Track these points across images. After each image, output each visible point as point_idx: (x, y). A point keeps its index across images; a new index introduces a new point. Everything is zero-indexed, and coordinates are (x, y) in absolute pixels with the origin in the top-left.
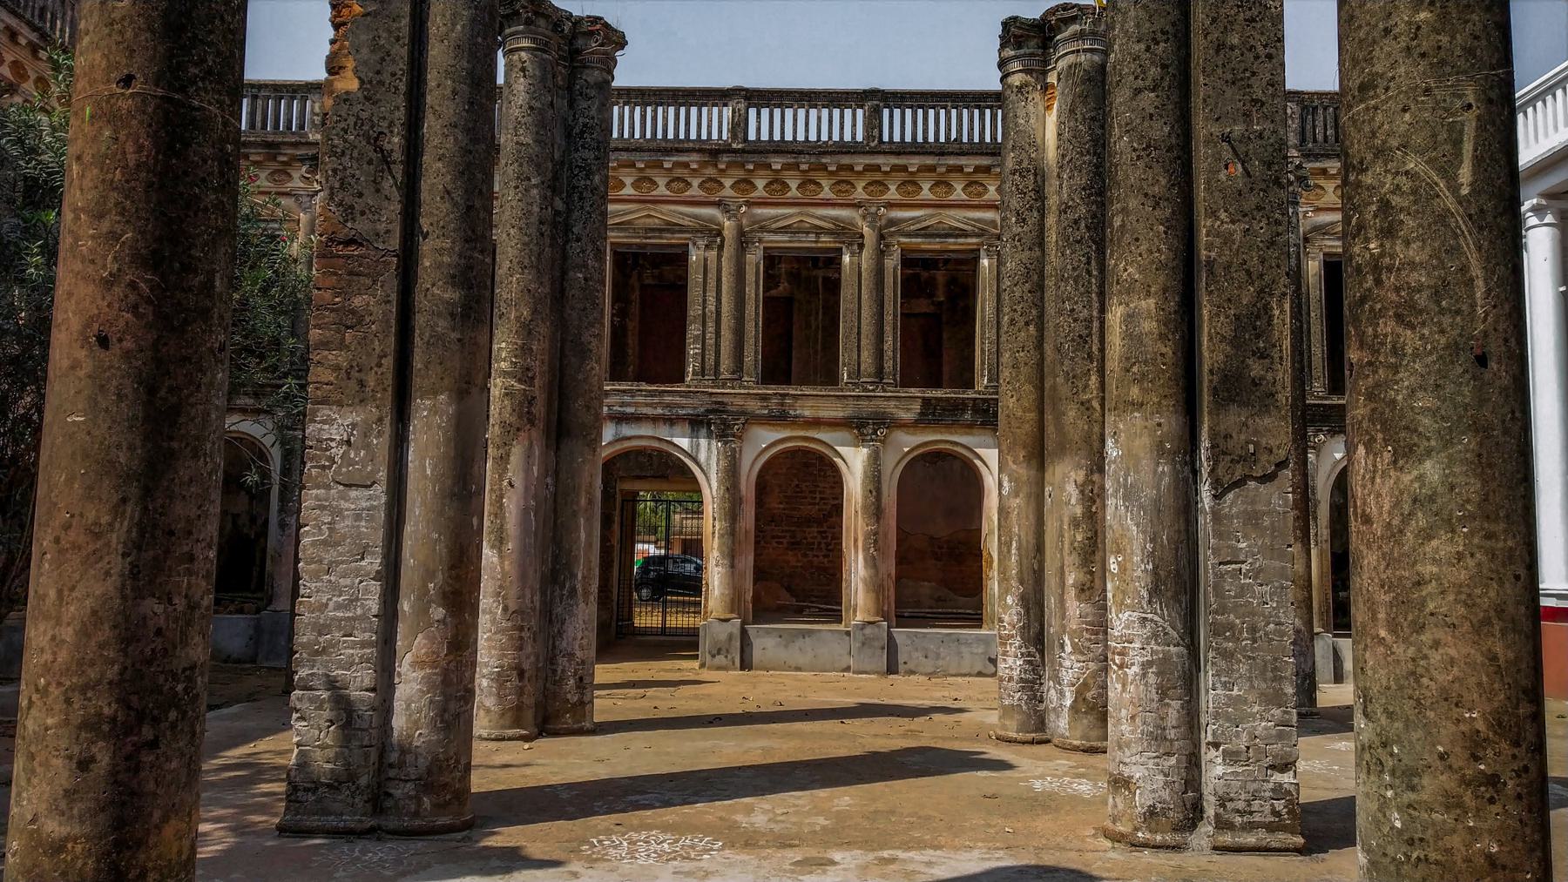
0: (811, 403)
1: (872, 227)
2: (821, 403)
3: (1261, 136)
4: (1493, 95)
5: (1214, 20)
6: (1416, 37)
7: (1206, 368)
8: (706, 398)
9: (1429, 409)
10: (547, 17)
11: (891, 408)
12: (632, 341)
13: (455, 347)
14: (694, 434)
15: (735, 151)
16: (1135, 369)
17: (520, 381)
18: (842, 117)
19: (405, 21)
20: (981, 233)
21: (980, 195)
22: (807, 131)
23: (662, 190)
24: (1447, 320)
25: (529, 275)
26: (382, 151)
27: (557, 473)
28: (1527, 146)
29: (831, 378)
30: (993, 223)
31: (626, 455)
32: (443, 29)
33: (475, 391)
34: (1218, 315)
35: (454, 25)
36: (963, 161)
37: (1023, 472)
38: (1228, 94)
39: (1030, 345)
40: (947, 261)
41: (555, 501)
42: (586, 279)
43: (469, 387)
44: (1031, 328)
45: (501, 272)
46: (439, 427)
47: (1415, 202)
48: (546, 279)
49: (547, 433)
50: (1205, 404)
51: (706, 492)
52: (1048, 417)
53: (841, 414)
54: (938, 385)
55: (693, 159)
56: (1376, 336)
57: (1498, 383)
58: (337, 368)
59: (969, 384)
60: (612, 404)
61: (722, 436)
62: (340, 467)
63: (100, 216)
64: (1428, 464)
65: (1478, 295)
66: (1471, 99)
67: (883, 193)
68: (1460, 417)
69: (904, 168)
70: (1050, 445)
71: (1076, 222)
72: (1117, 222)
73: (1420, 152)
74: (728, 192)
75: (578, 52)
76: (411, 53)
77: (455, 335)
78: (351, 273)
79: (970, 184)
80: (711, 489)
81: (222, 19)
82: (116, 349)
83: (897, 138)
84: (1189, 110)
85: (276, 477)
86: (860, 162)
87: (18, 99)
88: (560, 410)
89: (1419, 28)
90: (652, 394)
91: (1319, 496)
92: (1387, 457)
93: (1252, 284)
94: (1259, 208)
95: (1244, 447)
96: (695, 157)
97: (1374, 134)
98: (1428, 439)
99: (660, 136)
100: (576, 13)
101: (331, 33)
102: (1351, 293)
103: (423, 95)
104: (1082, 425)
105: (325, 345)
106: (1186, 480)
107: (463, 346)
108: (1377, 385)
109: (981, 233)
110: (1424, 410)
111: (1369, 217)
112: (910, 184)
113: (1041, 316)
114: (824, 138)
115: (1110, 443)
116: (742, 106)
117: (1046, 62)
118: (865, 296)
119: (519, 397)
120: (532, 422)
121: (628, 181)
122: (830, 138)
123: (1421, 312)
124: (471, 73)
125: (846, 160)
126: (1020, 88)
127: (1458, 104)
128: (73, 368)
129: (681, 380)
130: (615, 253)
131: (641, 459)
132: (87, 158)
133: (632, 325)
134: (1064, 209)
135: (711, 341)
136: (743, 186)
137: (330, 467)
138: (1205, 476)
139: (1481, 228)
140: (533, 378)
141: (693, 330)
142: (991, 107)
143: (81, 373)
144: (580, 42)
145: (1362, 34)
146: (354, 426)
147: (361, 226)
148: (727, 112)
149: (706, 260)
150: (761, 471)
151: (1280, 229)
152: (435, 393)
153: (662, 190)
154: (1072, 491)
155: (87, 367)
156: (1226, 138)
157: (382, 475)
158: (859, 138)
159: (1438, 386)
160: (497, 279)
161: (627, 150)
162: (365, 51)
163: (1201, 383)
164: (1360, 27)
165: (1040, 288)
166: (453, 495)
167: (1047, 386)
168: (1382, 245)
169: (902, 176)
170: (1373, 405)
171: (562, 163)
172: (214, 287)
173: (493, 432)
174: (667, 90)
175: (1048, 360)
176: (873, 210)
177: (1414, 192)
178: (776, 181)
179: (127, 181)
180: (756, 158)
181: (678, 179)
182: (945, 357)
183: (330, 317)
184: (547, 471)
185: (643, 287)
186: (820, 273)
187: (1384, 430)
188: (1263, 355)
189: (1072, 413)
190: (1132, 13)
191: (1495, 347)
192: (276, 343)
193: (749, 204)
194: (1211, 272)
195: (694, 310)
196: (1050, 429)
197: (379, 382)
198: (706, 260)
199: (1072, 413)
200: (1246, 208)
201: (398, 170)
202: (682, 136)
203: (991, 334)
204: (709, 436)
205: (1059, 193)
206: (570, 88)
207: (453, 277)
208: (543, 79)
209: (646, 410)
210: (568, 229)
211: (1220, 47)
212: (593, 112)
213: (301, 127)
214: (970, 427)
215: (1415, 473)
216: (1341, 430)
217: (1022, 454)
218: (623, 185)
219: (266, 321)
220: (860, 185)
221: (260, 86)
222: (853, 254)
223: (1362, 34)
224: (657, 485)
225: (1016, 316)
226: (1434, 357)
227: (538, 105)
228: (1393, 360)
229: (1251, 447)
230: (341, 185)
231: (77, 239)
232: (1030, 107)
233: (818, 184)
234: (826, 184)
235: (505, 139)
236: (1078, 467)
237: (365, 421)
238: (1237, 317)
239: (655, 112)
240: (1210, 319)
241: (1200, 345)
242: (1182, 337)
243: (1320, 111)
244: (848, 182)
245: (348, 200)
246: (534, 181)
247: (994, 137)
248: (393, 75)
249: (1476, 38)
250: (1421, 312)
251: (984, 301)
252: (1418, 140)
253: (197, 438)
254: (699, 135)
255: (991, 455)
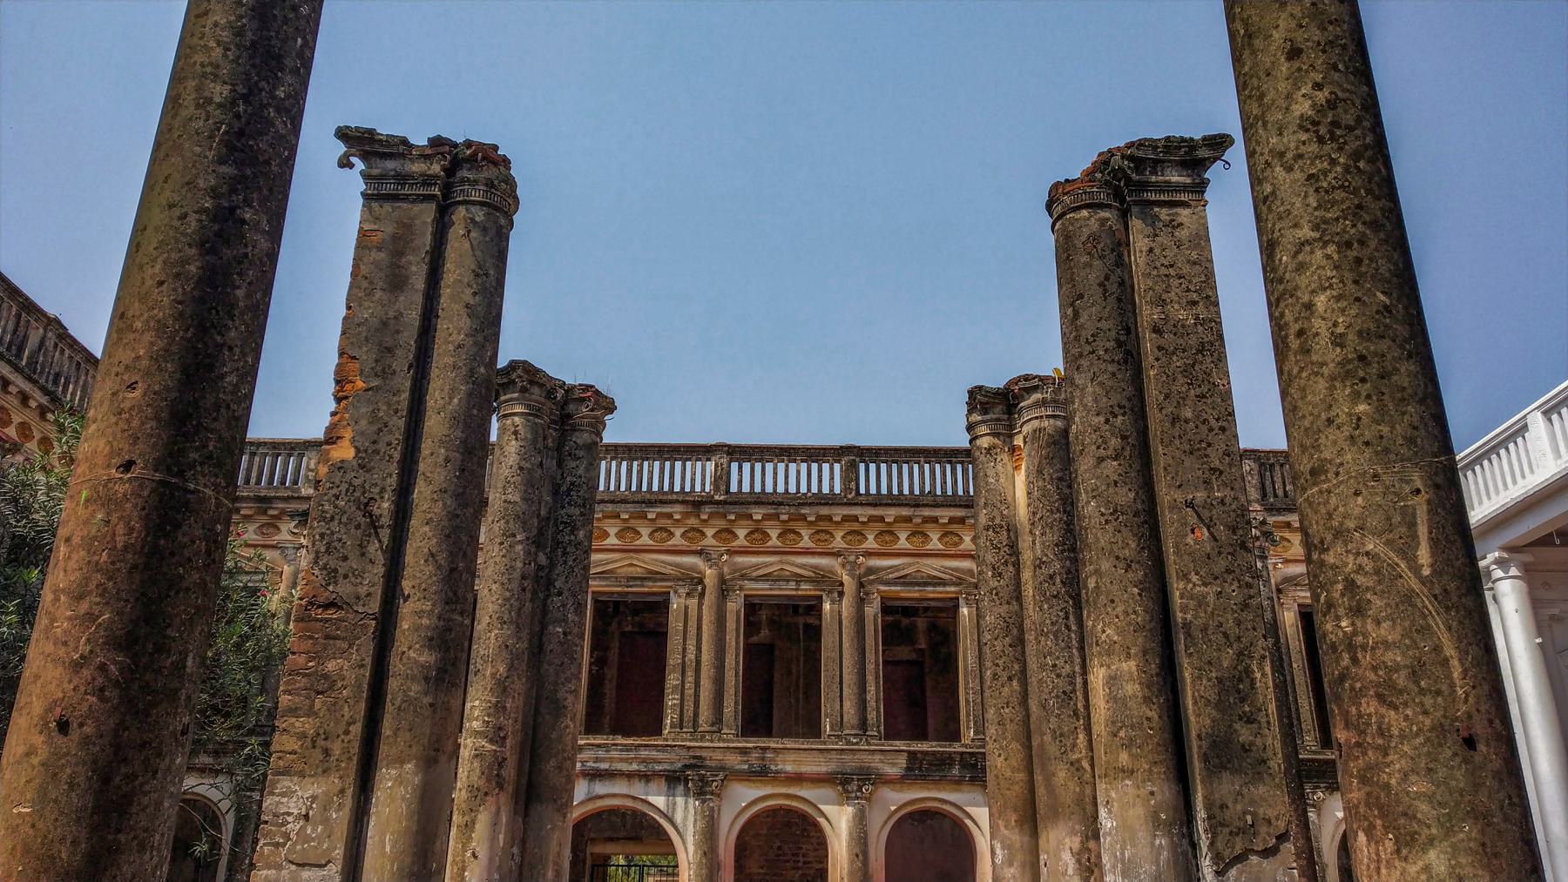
0: (793, 756)
1: (852, 576)
2: (808, 757)
3: (1222, 502)
4: (1440, 480)
5: (1167, 397)
6: (1358, 427)
7: (1194, 734)
8: (684, 752)
9: (1424, 794)
10: (542, 386)
11: (875, 762)
12: (610, 689)
13: (428, 712)
14: (670, 792)
15: (718, 503)
16: (1122, 734)
17: (491, 741)
18: (820, 470)
19: (406, 395)
20: (959, 582)
21: (956, 544)
22: (787, 483)
23: (645, 540)
24: (1428, 701)
25: (508, 631)
26: (371, 516)
27: (523, 842)
28: (1481, 503)
29: (814, 731)
30: (970, 572)
31: (598, 815)
32: (441, 402)
33: (443, 758)
34: (1200, 678)
35: (451, 399)
36: (937, 512)
37: (1016, 837)
38: (1187, 463)
39: (1015, 700)
40: (926, 609)
41: (521, 874)
42: (565, 634)
43: (437, 755)
44: (1015, 683)
45: (480, 627)
46: (403, 799)
47: (1380, 582)
48: (525, 634)
49: (516, 796)
50: (1197, 771)
51: (682, 856)
52: (1038, 778)
53: (824, 769)
54: (923, 736)
55: (677, 510)
56: (1360, 716)
57: (1489, 766)
58: (303, 736)
59: (955, 736)
60: (586, 759)
61: (700, 794)
62: (295, 844)
63: (80, 598)
64: (1432, 854)
65: (1456, 675)
66: (1419, 484)
67: (861, 542)
68: (1458, 804)
69: (881, 519)
70: (1042, 809)
71: (1051, 577)
72: (1091, 583)
73: (1378, 534)
74: (709, 541)
75: (569, 416)
76: (408, 424)
77: (427, 700)
78: (327, 637)
79: (945, 534)
80: (688, 853)
81: (228, 407)
82: (75, 734)
83: (873, 490)
84: (1151, 477)
85: (226, 846)
86: (838, 513)
87: (19, 458)
88: (530, 773)
89: (1359, 419)
90: (627, 748)
91: (1325, 860)
92: (1390, 845)
93: (1231, 646)
94: (1228, 571)
95: (1242, 818)
96: (678, 508)
97: (1330, 515)
98: (1429, 827)
99: (644, 488)
100: (569, 381)
101: (333, 406)
102: (1330, 672)
103: (417, 463)
104: (1073, 787)
105: (293, 711)
106: (1185, 854)
107: (434, 712)
108: (1369, 767)
109: (959, 582)
110: (1419, 796)
111: (1337, 595)
112: (888, 533)
113: (1024, 671)
114: (803, 489)
115: (1103, 812)
116: (725, 461)
117: (1012, 427)
118: (846, 645)
119: (489, 759)
120: (500, 786)
121: (612, 531)
122: (809, 490)
123: (1401, 692)
124: (464, 442)
125: (824, 511)
126: (989, 450)
127: (1407, 489)
128: (28, 754)
129: (657, 730)
130: (596, 601)
131: (614, 819)
132: (76, 540)
133: (611, 673)
134: (1039, 565)
135: (690, 692)
136: (725, 535)
137: (284, 845)
138: (1205, 849)
139: (1448, 609)
140: (504, 738)
141: (672, 680)
142: (962, 463)
143: (35, 761)
144: (571, 407)
145: (1306, 423)
146: (314, 798)
147: (344, 589)
148: (710, 466)
149: (686, 608)
150: (738, 838)
151: (1252, 592)
152: (401, 761)
153: (645, 540)
154: (1068, 859)
155: (43, 753)
156: (1190, 504)
157: (339, 853)
158: (837, 490)
159: (1430, 770)
160: (475, 634)
161: (612, 502)
162: (363, 422)
163: (1190, 749)
164: (1304, 416)
165: (1020, 642)
166: (412, 874)
167: (1035, 744)
168: (1353, 624)
169: (880, 526)
170: (1368, 789)
171: (548, 519)
172: (184, 667)
173: (460, 795)
174: (652, 446)
175: (1033, 718)
176: (852, 558)
177: (1377, 572)
178: (757, 530)
179: (113, 563)
180: (738, 509)
181: (661, 529)
182: (930, 709)
183: (302, 682)
184: (513, 839)
185: (624, 634)
186: (801, 620)
187: (1383, 816)
188: (1250, 720)
189: (1062, 774)
190: (1090, 389)
191: (1480, 728)
192: (244, 701)
193: (731, 553)
194: (1188, 635)
195: (673, 659)
196: (1041, 791)
197: (346, 751)
198: (686, 608)
199: (1062, 774)
200: (1216, 570)
201: (385, 534)
202: (666, 488)
203: (974, 684)
204: (686, 794)
205: (1033, 549)
206: (559, 448)
207: (431, 639)
208: (534, 442)
209: (624, 767)
210: (550, 583)
211: (1175, 420)
212: (581, 471)
213: (295, 482)
214: (958, 783)
215: (1420, 863)
216: (1338, 789)
217: (1014, 817)
218: (606, 535)
219: (235, 679)
220: (839, 535)
221: (259, 444)
222: (833, 602)
223: (1306, 423)
224: (631, 847)
225: (999, 670)
226: (1421, 740)
227: (527, 465)
228: (1380, 741)
229: (1249, 818)
230: (328, 548)
231: (53, 620)
232: (999, 467)
233: (799, 534)
234: (805, 533)
235: (495, 497)
236: (1073, 833)
237: (326, 793)
238: (1220, 680)
239: (641, 466)
240: (1193, 681)
241: (1186, 709)
242: (1167, 700)
243: (1277, 468)
244: (827, 532)
245: (332, 564)
246: (519, 537)
247: (966, 490)
248: (389, 444)
249: (1415, 428)
250: (1401, 692)
251: (965, 650)
252: (1374, 522)
253: (146, 830)
254: (683, 488)
255: (981, 814)
